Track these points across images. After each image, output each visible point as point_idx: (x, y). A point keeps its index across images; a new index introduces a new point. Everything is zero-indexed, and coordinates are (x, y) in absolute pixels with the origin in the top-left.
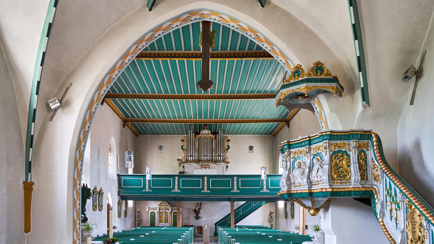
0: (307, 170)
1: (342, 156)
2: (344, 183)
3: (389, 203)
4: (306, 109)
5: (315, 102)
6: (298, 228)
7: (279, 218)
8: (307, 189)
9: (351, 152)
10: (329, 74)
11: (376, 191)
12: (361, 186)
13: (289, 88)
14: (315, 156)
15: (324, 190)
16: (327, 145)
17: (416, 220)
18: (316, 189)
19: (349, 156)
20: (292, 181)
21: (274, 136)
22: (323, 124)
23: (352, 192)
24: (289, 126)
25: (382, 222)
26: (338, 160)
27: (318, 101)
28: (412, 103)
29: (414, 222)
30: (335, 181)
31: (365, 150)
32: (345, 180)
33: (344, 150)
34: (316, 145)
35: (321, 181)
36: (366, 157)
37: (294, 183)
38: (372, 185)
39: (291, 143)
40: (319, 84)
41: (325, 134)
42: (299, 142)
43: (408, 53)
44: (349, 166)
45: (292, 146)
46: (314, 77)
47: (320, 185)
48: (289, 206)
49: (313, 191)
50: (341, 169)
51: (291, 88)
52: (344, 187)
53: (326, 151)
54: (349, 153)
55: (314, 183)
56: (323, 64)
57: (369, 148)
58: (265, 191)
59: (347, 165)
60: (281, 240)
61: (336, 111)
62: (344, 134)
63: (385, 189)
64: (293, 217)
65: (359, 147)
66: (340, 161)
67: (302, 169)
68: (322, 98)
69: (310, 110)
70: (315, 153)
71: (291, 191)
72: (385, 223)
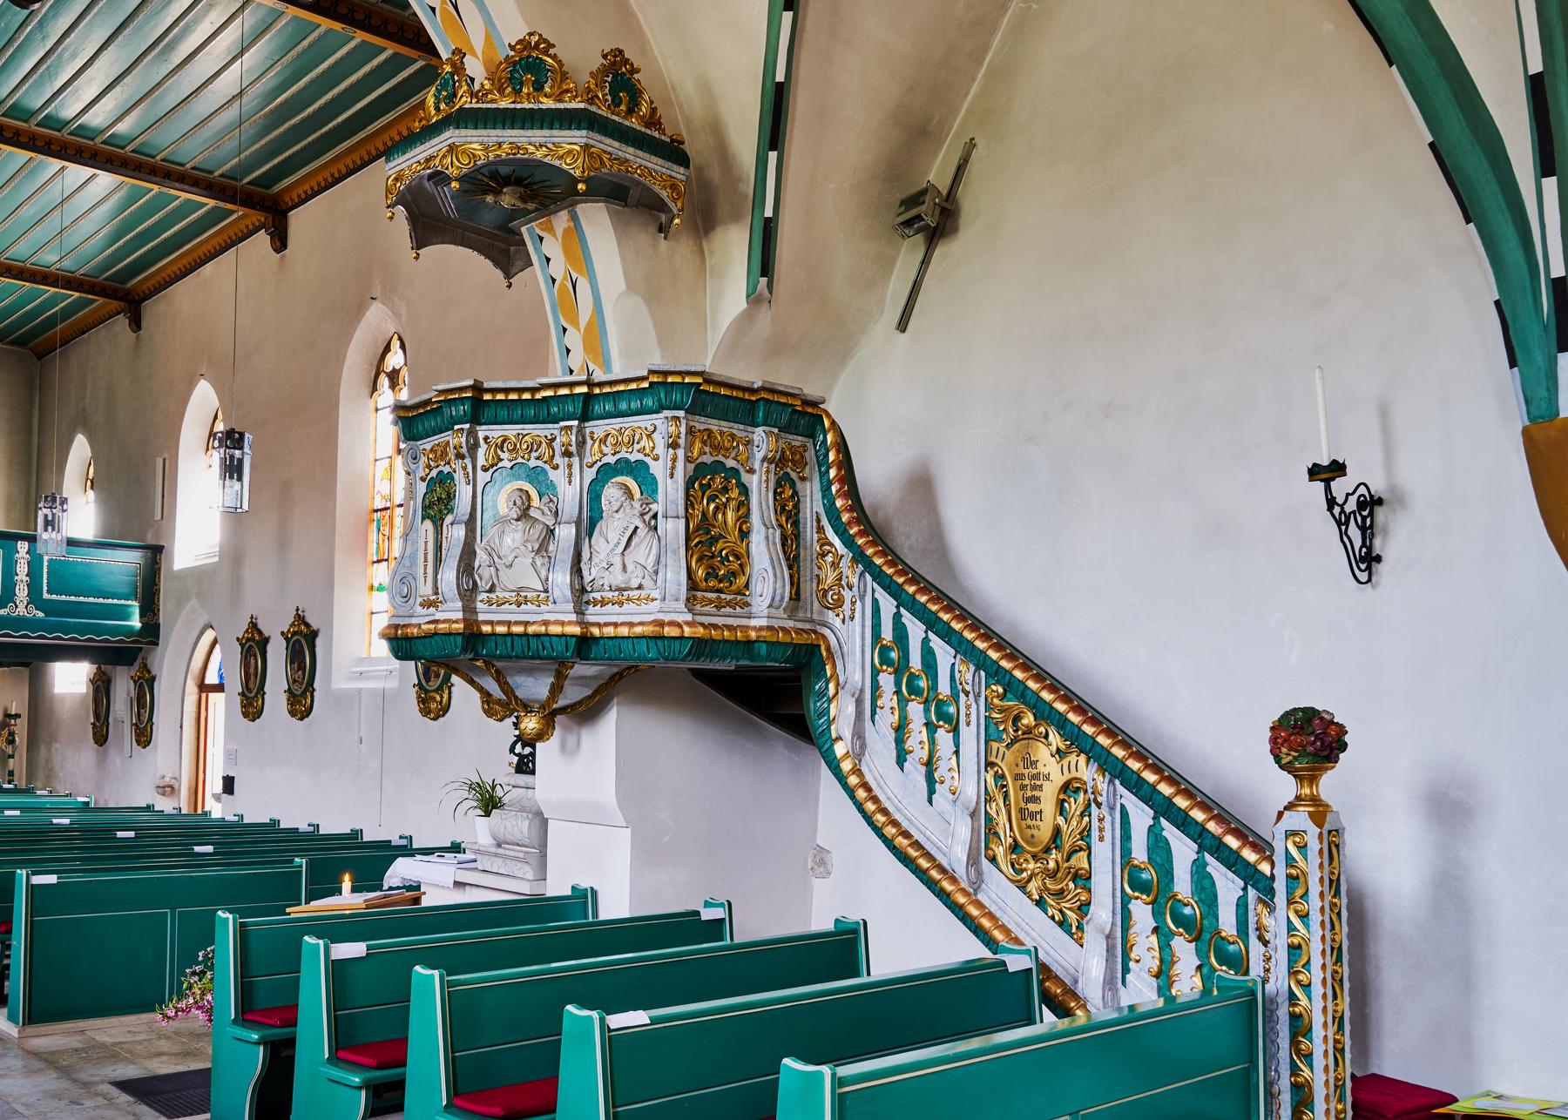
0: (566, 533)
1: (725, 490)
2: (728, 604)
3: (888, 699)
4: (481, 252)
5: (551, 230)
6: (168, 790)
7: (53, 739)
8: (460, 615)
9: (755, 478)
10: (653, 121)
11: (828, 649)
12: (689, 617)
13: (499, 132)
14: (606, 472)
15: (669, 631)
16: (683, 429)
17: (1041, 768)
18: (616, 625)
19: (745, 491)
20: (484, 575)
21: (43, 353)
22: (574, 339)
23: (764, 646)
24: (136, 324)
25: (856, 771)
26: (712, 506)
27: (567, 231)
28: (903, 325)
29: (1036, 776)
30: (699, 594)
31: (793, 475)
32: (731, 593)
33: (730, 463)
34: (617, 423)
35: (640, 587)
36: (796, 506)
37: (492, 590)
38: (811, 621)
39: (487, 397)
40: (629, 153)
41: (678, 379)
42: (526, 396)
43: (916, 129)
44: (744, 534)
45: (489, 413)
46: (604, 112)
47: (628, 607)
48: (123, 687)
49: (596, 631)
50: (720, 545)
51: (510, 132)
52: (730, 621)
53: (674, 460)
54: (745, 477)
55: (597, 596)
56: (634, 71)
57: (806, 473)
58: (21, 610)
59: (741, 530)
60: (210, 849)
61: (648, 288)
62: (550, 393)
63: (868, 641)
64: (144, 736)
65: (779, 461)
66: (717, 508)
67: (539, 527)
68: (596, 220)
69: (497, 264)
70: (611, 460)
71: (478, 623)
72: (869, 778)
